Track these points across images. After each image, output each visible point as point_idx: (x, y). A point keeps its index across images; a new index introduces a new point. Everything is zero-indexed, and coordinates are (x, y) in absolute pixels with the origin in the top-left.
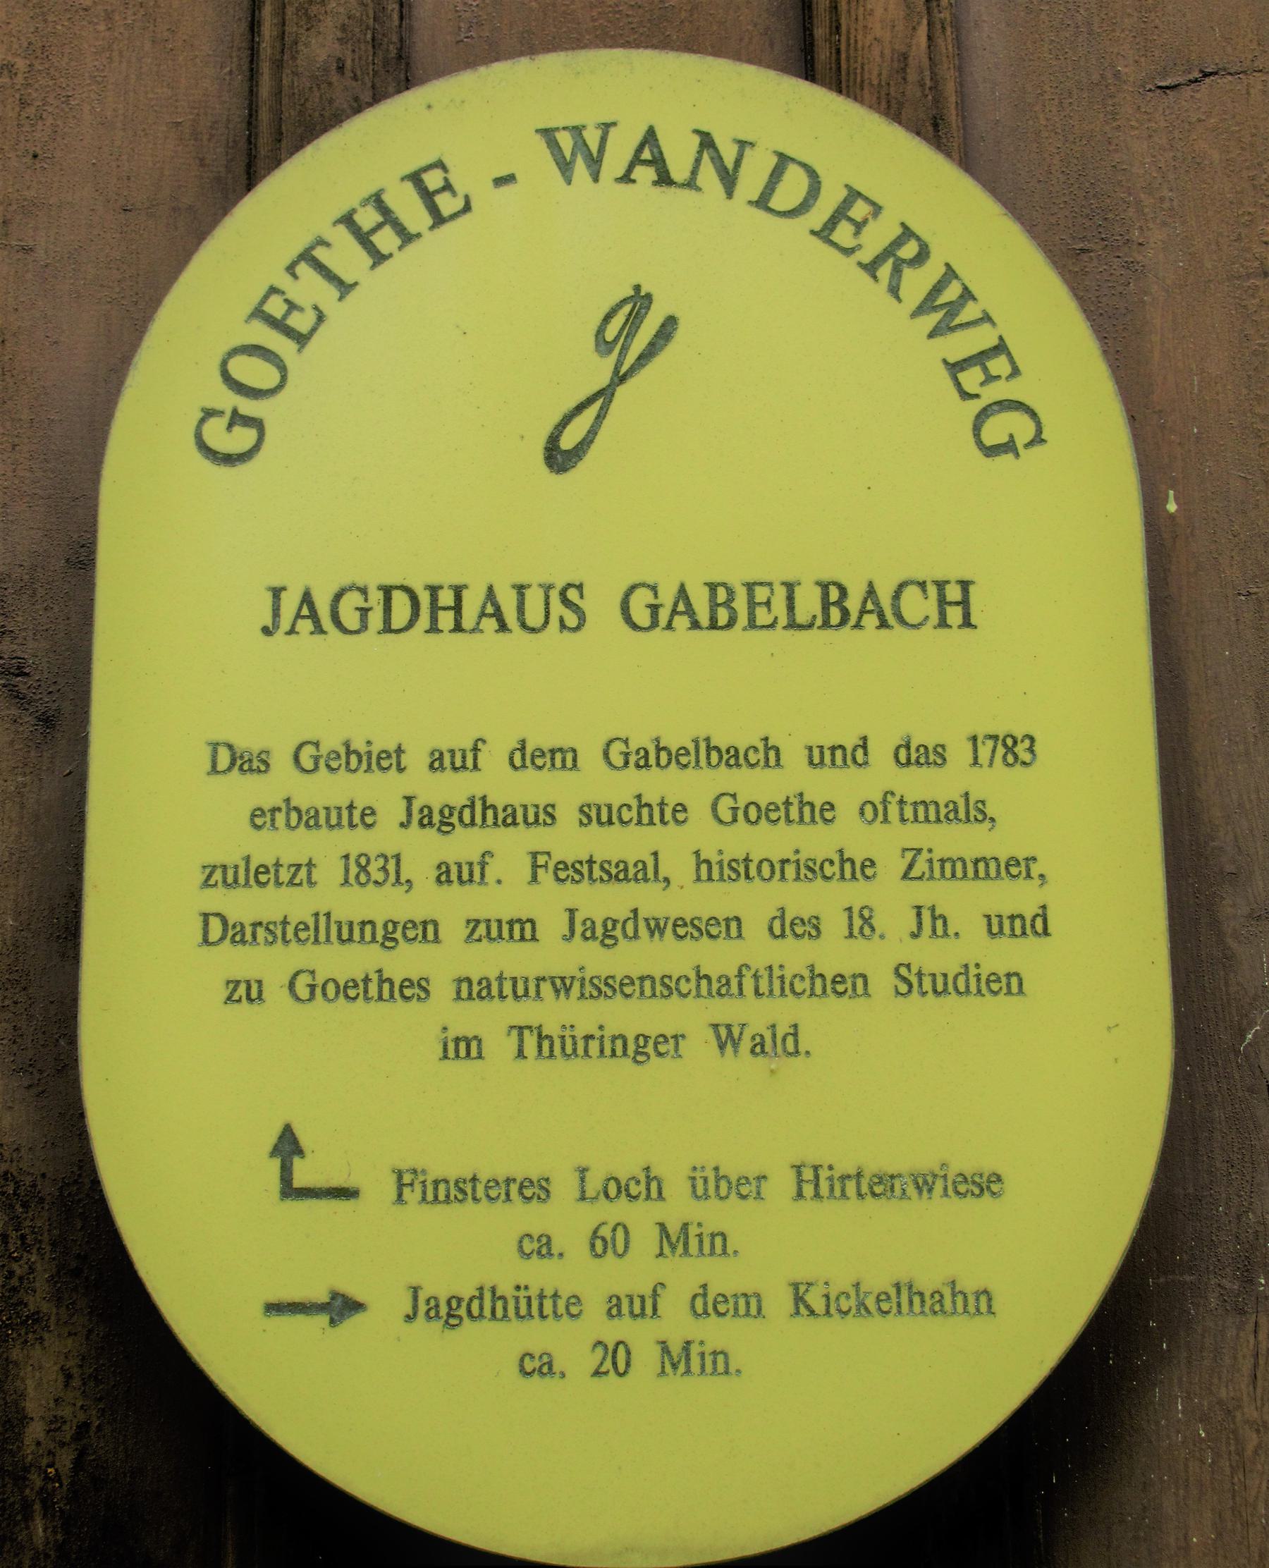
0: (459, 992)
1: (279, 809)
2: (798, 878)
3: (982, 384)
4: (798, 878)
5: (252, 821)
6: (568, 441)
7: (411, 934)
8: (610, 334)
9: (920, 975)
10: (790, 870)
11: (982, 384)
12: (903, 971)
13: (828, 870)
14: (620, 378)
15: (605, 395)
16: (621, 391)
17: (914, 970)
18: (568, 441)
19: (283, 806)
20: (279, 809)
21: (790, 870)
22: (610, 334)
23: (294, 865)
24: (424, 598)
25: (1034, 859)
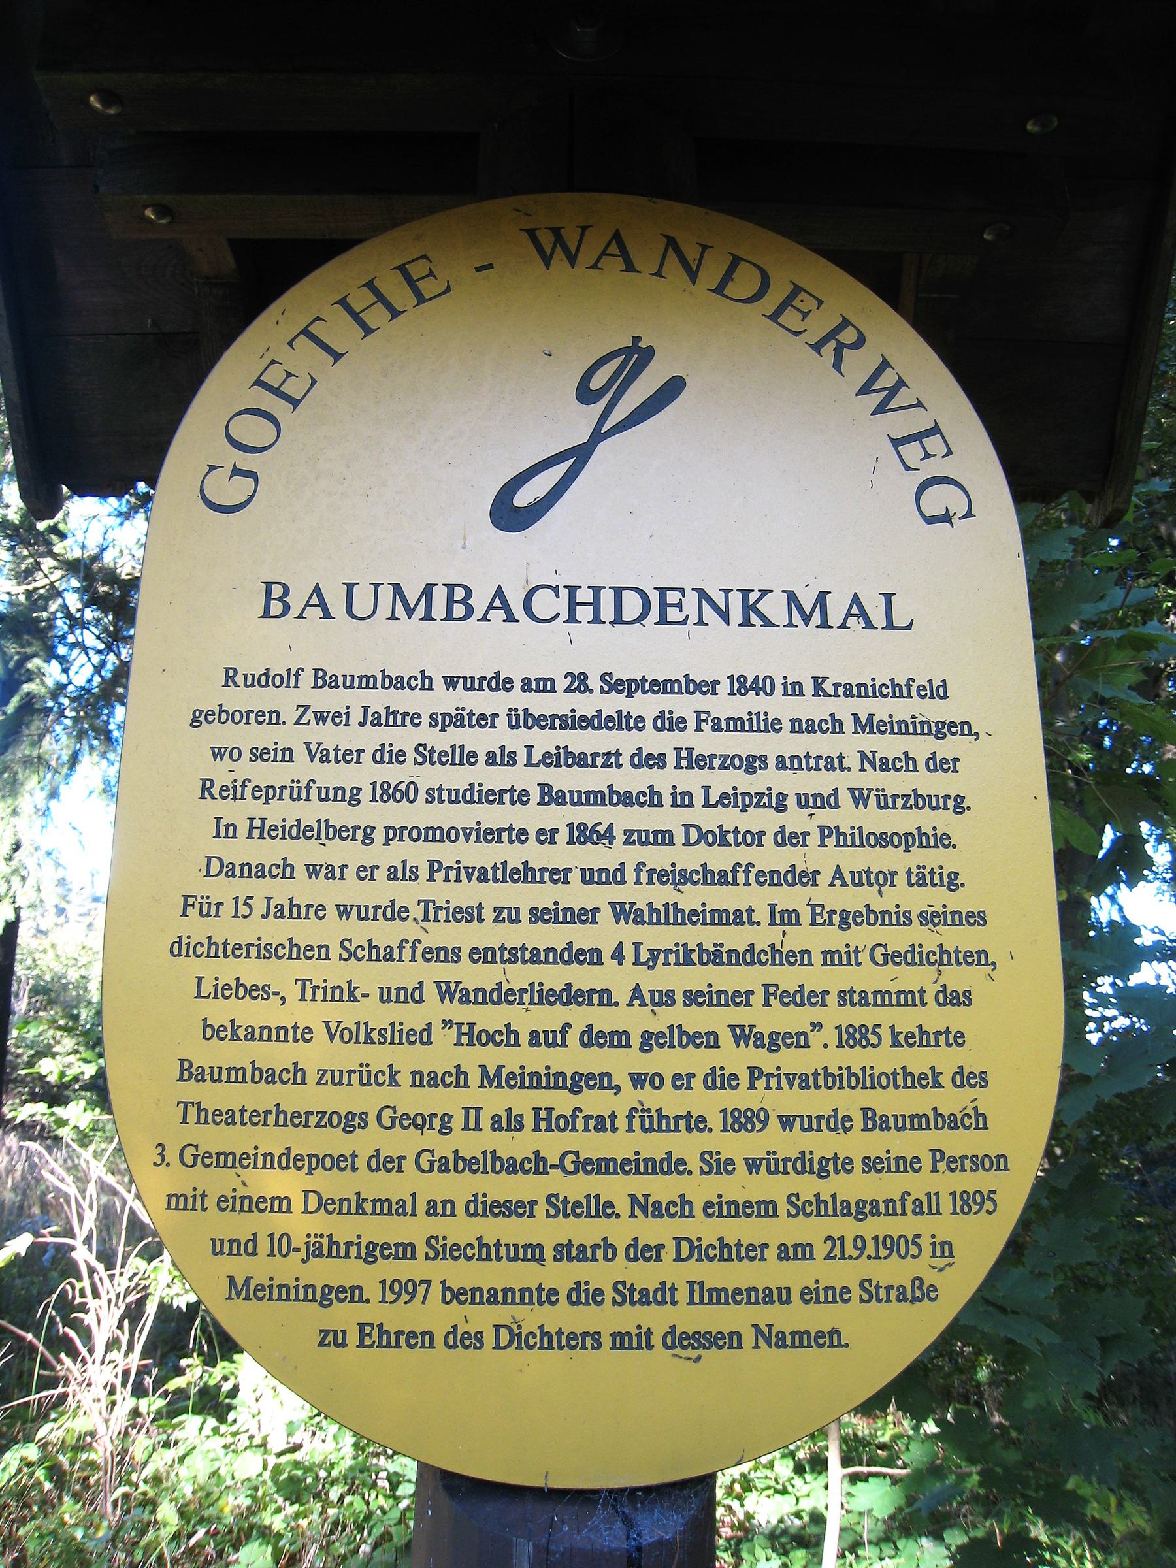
0: (169, 1203)
1: (271, 1112)
2: (258, 957)
3: (681, 611)
4: (258, 957)
5: (218, 1205)
6: (523, 498)
7: (342, 1296)
8: (596, 383)
9: (878, 1287)
10: (253, 951)
11: (681, 611)
12: (866, 1285)
13: (280, 952)
14: (597, 437)
15: (580, 455)
16: (602, 448)
17: (874, 1284)
18: (523, 498)
19: (274, 1110)
20: (271, 1112)
21: (253, 951)
22: (596, 383)
23: (325, 1345)
24: (654, 598)
25: (222, 904)
